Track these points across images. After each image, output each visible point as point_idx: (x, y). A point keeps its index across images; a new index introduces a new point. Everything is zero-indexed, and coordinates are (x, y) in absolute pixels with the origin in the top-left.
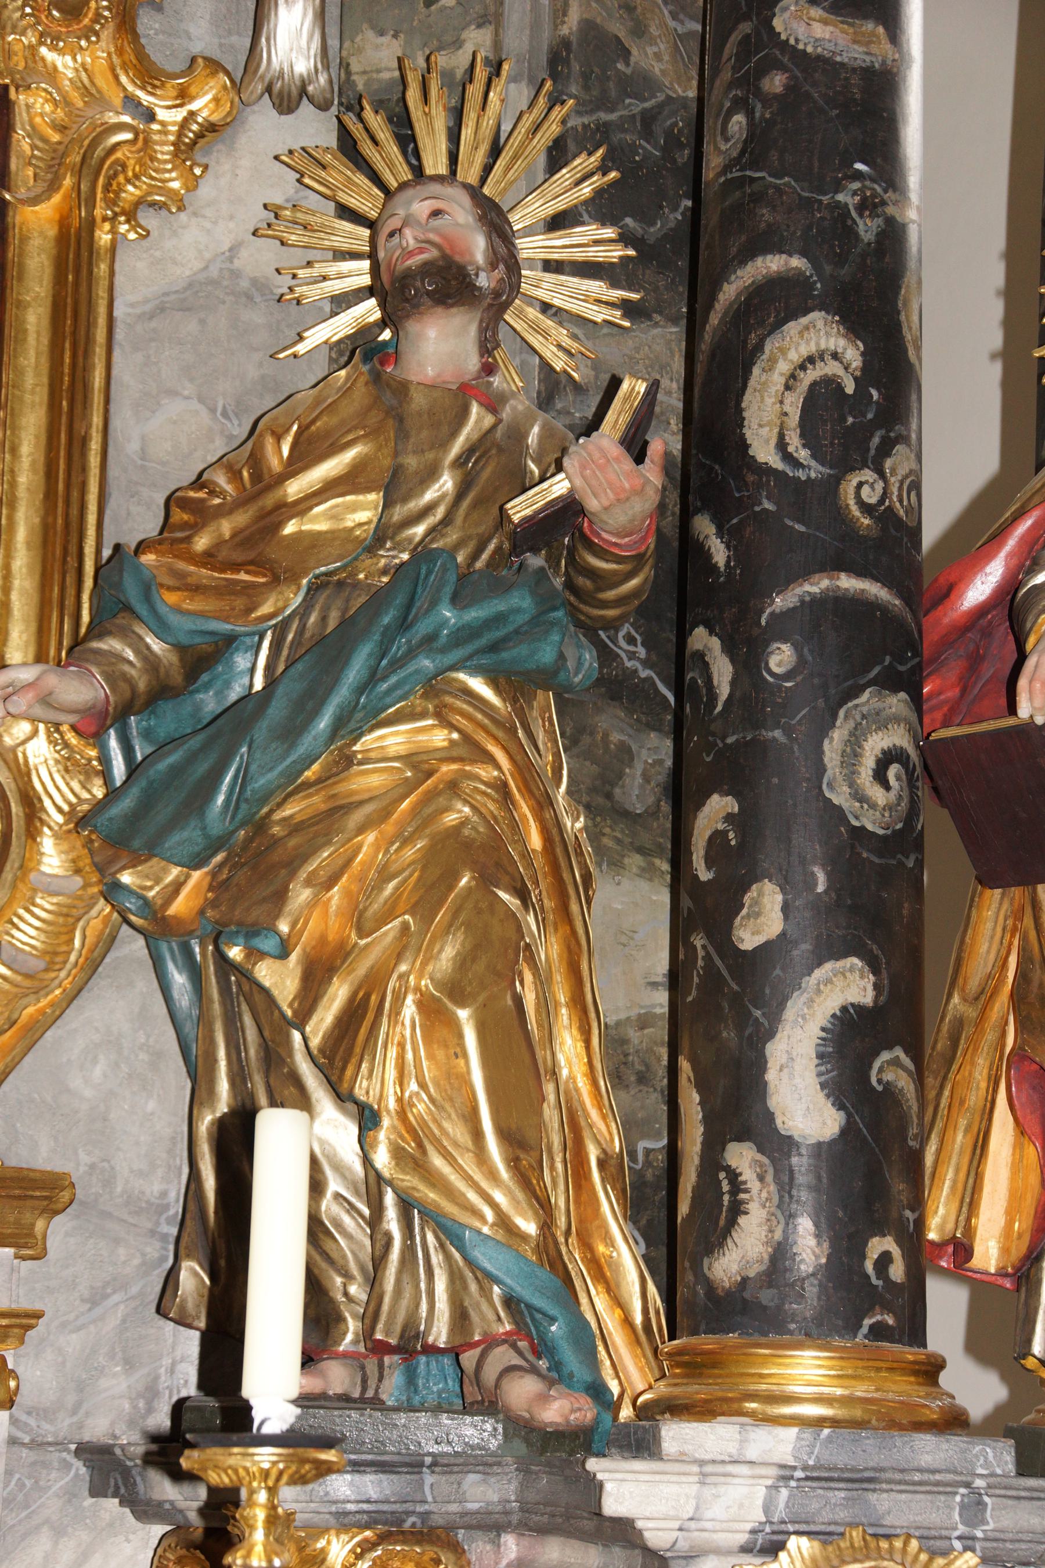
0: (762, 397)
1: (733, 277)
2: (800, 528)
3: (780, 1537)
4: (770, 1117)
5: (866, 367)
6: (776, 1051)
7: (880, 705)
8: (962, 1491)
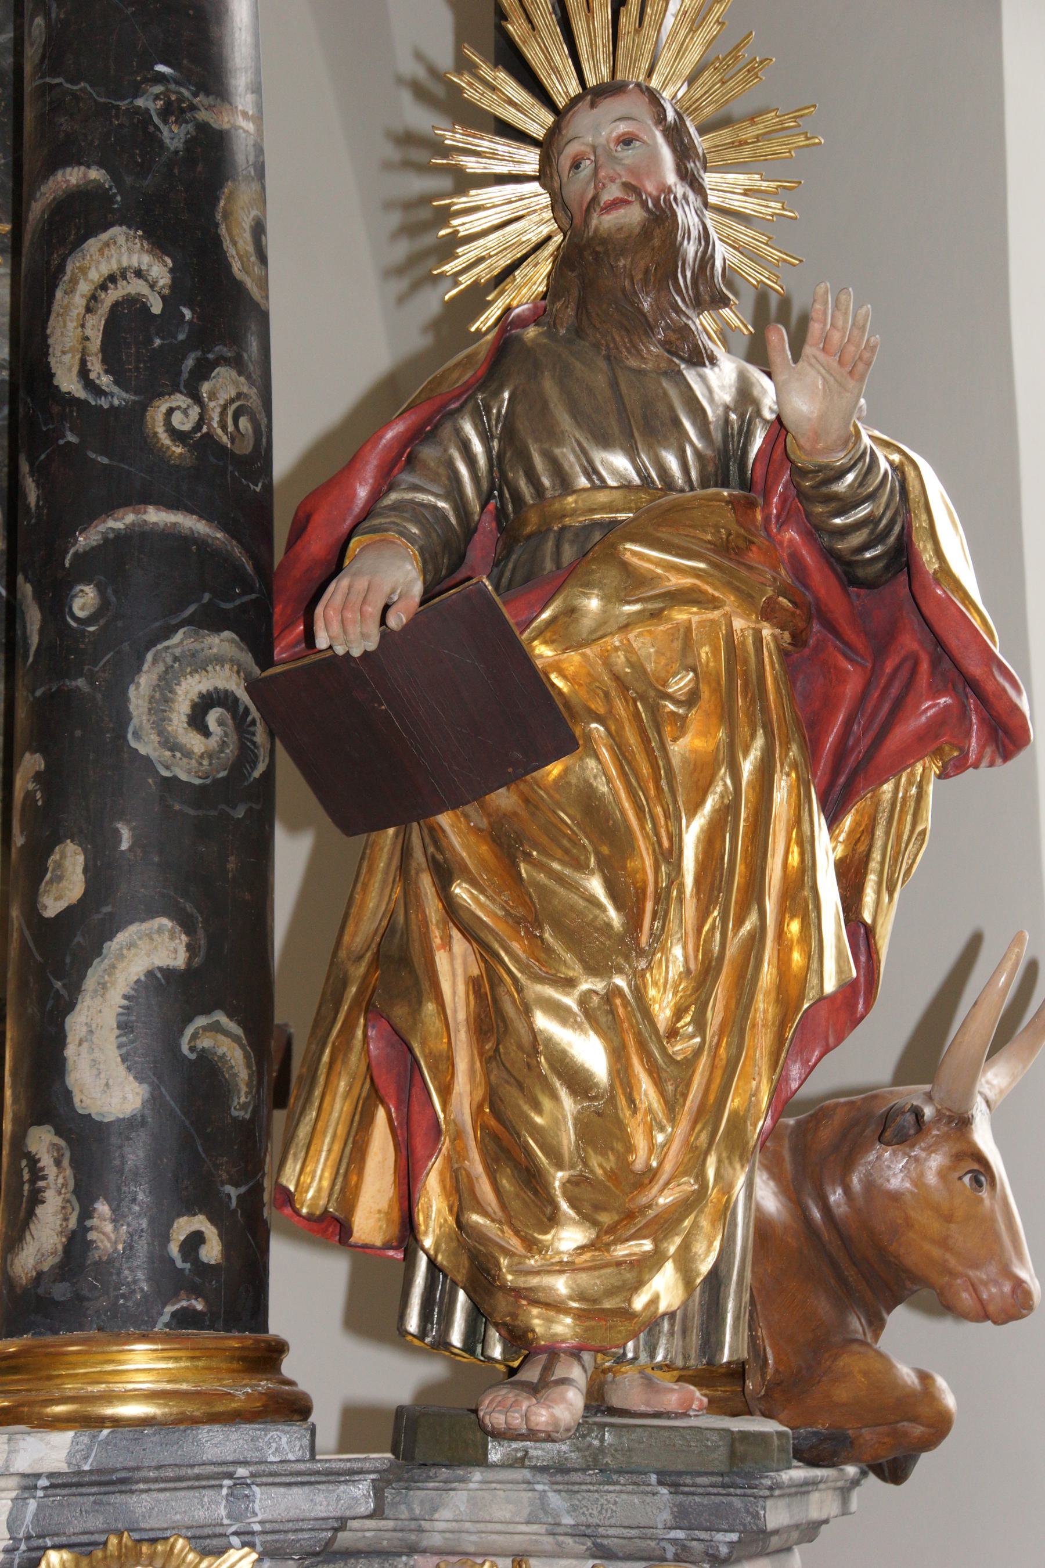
0: (65, 322)
1: (38, 195)
2: (105, 460)
3: (34, 1555)
4: (68, 1094)
5: (174, 286)
6: (76, 1024)
7: (197, 646)
8: (227, 1482)
